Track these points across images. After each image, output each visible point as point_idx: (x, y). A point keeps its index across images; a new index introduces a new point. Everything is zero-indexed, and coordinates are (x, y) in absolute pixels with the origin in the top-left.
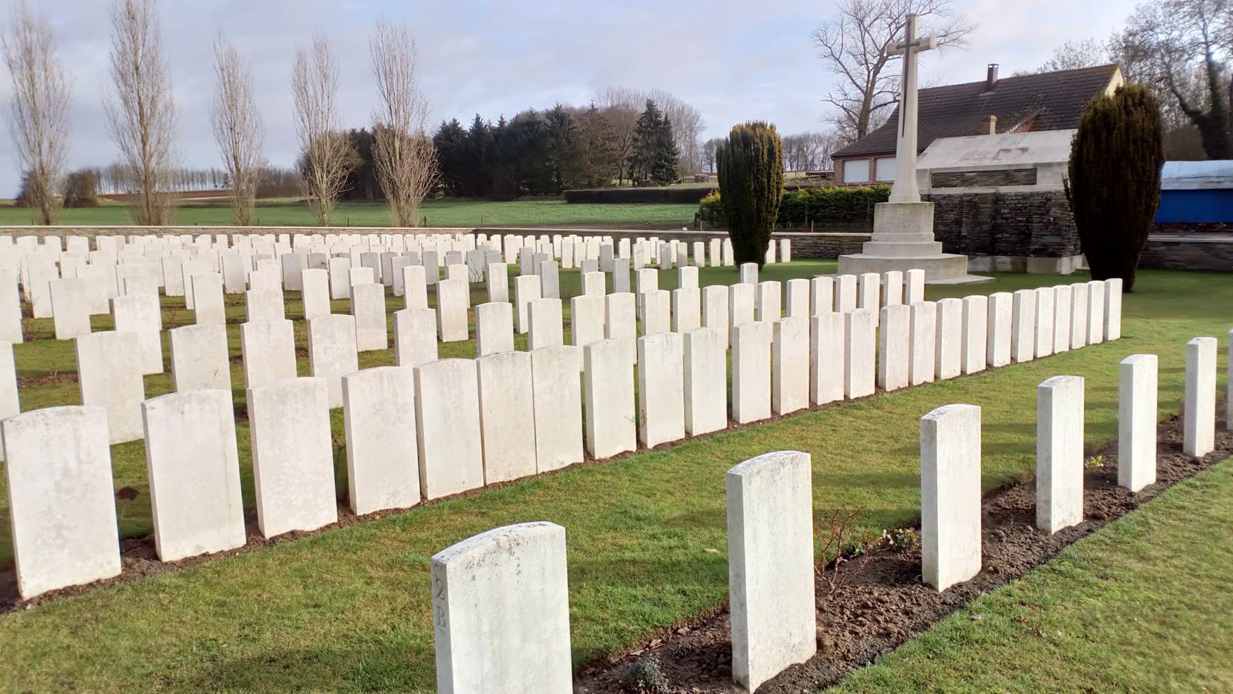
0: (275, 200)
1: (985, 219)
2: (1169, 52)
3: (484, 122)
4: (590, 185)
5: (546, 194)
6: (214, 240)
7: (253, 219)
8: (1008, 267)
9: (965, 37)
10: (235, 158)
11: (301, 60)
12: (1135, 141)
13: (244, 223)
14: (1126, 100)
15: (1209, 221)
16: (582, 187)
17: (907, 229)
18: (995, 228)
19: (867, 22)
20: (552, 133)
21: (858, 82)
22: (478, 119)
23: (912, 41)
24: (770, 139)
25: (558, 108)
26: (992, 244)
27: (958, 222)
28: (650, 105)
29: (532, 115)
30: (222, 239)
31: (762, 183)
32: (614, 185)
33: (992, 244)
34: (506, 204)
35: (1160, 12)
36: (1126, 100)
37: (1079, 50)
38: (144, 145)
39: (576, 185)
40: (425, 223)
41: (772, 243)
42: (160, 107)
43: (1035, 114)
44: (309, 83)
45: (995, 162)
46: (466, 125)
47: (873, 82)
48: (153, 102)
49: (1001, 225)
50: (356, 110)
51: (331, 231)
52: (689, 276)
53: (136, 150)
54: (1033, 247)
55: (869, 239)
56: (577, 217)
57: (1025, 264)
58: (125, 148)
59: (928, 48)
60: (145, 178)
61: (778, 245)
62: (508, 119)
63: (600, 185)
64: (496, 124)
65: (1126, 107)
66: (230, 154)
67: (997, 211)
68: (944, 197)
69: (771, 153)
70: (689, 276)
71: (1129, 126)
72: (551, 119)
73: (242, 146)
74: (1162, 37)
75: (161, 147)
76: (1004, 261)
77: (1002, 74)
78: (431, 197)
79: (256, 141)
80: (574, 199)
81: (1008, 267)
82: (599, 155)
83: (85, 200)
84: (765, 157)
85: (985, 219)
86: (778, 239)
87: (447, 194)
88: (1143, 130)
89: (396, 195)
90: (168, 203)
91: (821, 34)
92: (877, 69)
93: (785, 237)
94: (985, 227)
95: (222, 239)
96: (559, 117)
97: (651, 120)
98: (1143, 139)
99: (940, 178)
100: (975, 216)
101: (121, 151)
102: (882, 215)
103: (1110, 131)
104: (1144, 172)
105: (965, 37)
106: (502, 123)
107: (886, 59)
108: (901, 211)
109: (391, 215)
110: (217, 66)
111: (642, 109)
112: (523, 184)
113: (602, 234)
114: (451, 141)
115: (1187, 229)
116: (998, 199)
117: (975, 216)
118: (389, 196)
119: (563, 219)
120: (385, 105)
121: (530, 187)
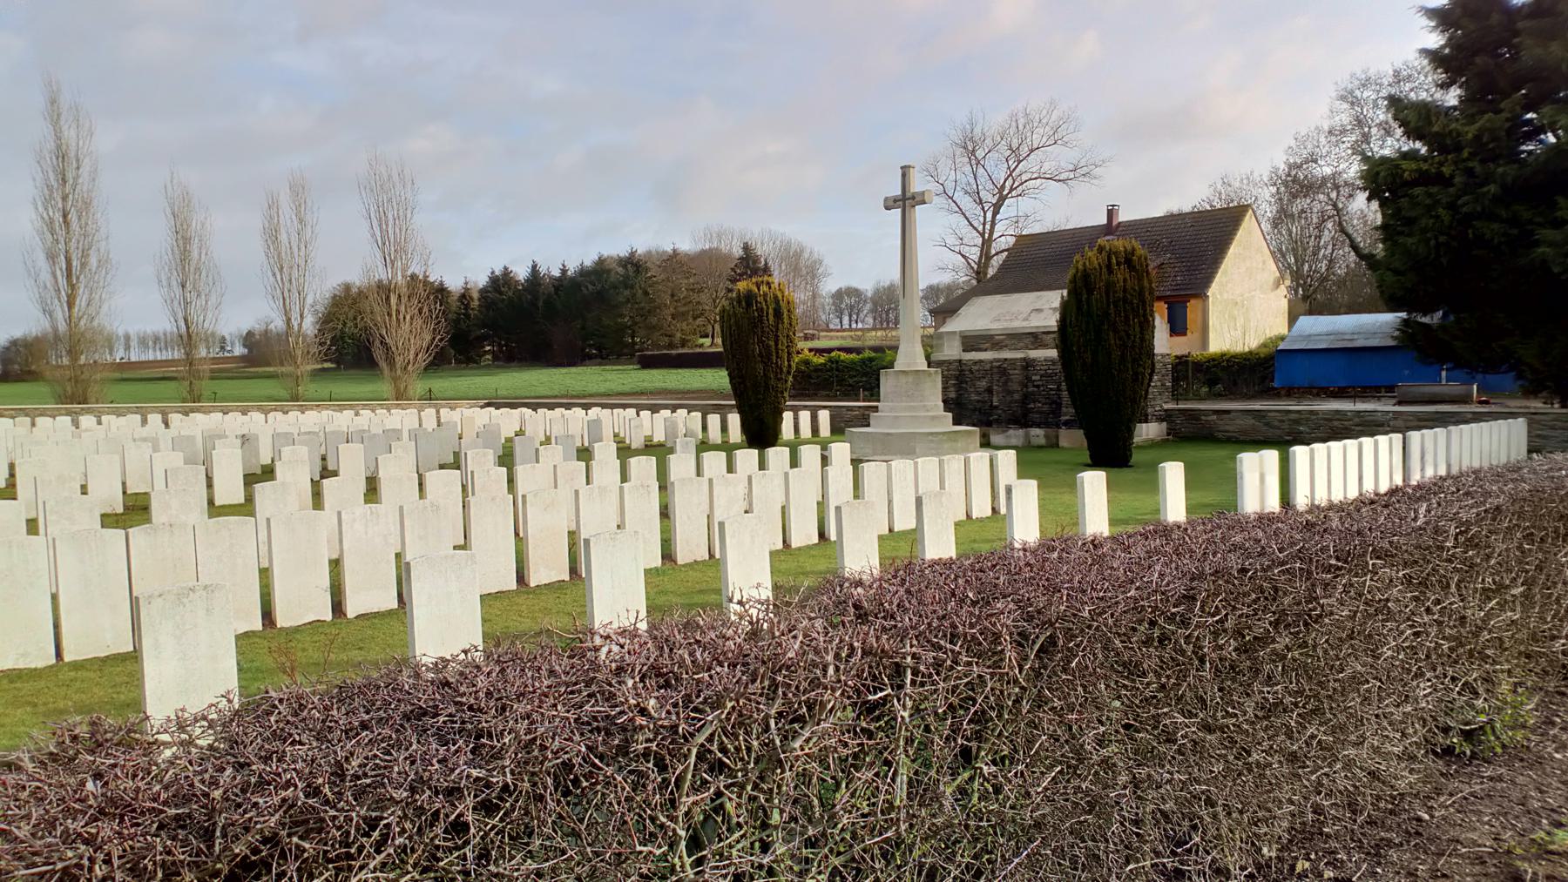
0: (260, 369)
1: (1016, 387)
2: (1336, 187)
3: (543, 270)
4: (671, 346)
5: (619, 356)
6: (144, 422)
7: (206, 393)
8: (1042, 441)
9: (1097, 171)
10: (186, 321)
11: (273, 205)
12: (1116, 304)
13: (193, 400)
14: (1109, 258)
15: (1343, 384)
16: (659, 347)
17: (913, 399)
18: (1026, 398)
19: (980, 154)
20: (626, 283)
21: (976, 224)
22: (534, 267)
23: (908, 195)
24: (776, 297)
25: (633, 254)
26: (1025, 415)
27: (989, 391)
28: (746, 248)
29: (347, 287)
30: (155, 419)
31: (769, 346)
32: (701, 346)
33: (1025, 415)
34: (564, 370)
35: (1323, 140)
36: (1109, 258)
37: (1237, 184)
38: (70, 305)
39: (657, 346)
40: (430, 397)
41: (788, 416)
42: (93, 261)
43: (1158, 262)
44: (283, 231)
45: (1025, 324)
46: (521, 273)
47: (993, 224)
48: (85, 255)
49: (1033, 393)
50: (344, 260)
51: (364, 407)
52: (605, 453)
53: (60, 316)
54: (1064, 418)
55: (876, 409)
56: (647, 385)
57: (1057, 437)
58: (48, 312)
59: (924, 202)
60: (74, 341)
61: (796, 419)
62: (572, 268)
63: (683, 346)
64: (556, 273)
65: (1109, 266)
66: (180, 315)
67: (1028, 378)
68: (975, 363)
69: (778, 314)
70: (605, 453)
71: (1109, 286)
72: (625, 267)
73: (197, 304)
74: (1328, 171)
75: (91, 310)
76: (1038, 435)
77: (1123, 216)
78: (438, 362)
79: (213, 300)
80: (648, 363)
81: (1042, 441)
82: (682, 309)
83: (30, 372)
84: (771, 318)
85: (1016, 387)
86: (796, 410)
87: (496, 358)
88: (1125, 290)
89: (391, 362)
90: (98, 376)
91: (932, 169)
92: (997, 208)
93: (805, 408)
94: (1016, 396)
95: (155, 419)
96: (633, 265)
97: (747, 267)
98: (1125, 300)
99: (971, 342)
100: (1006, 383)
101: (41, 315)
102: (887, 382)
103: (1090, 292)
104: (1128, 336)
105: (1097, 171)
106: (564, 271)
107: (1006, 197)
108: (903, 379)
109: (385, 387)
110: (168, 211)
111: (738, 252)
112: (590, 346)
113: (624, 407)
114: (501, 293)
115: (1318, 395)
116: (1028, 364)
117: (1006, 383)
118: (383, 364)
119: (603, 388)
120: (379, 255)
121: (599, 349)
